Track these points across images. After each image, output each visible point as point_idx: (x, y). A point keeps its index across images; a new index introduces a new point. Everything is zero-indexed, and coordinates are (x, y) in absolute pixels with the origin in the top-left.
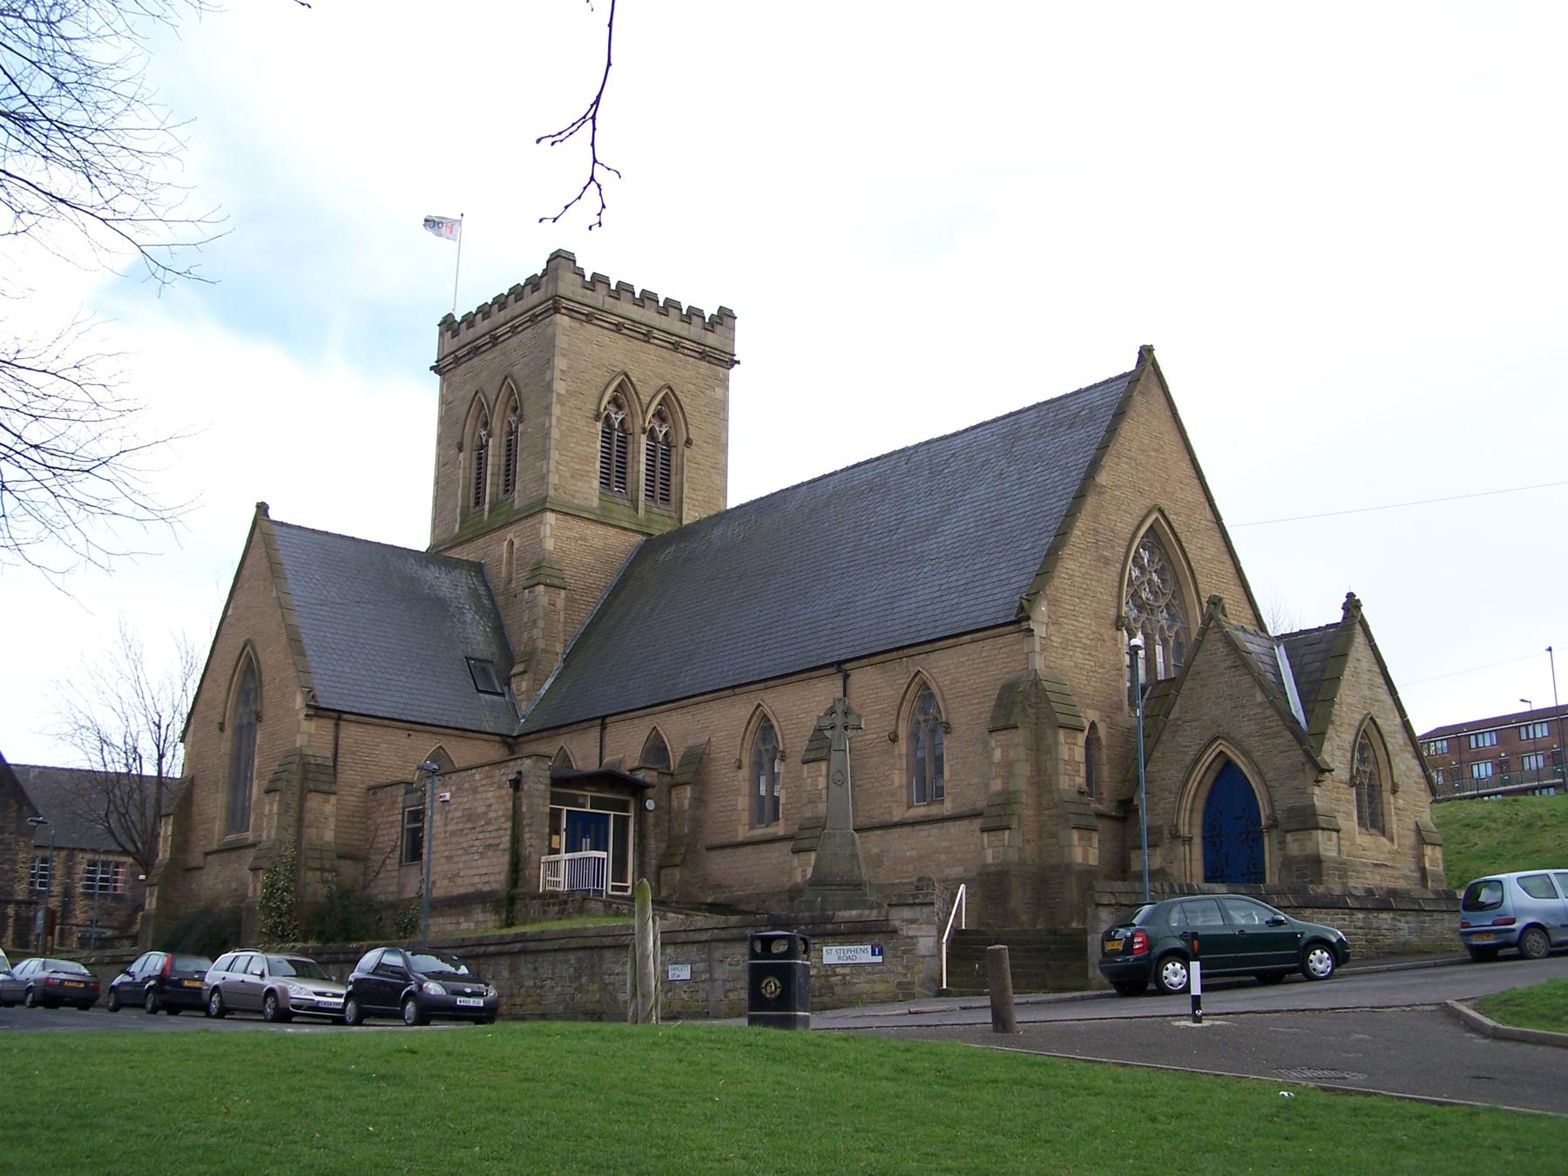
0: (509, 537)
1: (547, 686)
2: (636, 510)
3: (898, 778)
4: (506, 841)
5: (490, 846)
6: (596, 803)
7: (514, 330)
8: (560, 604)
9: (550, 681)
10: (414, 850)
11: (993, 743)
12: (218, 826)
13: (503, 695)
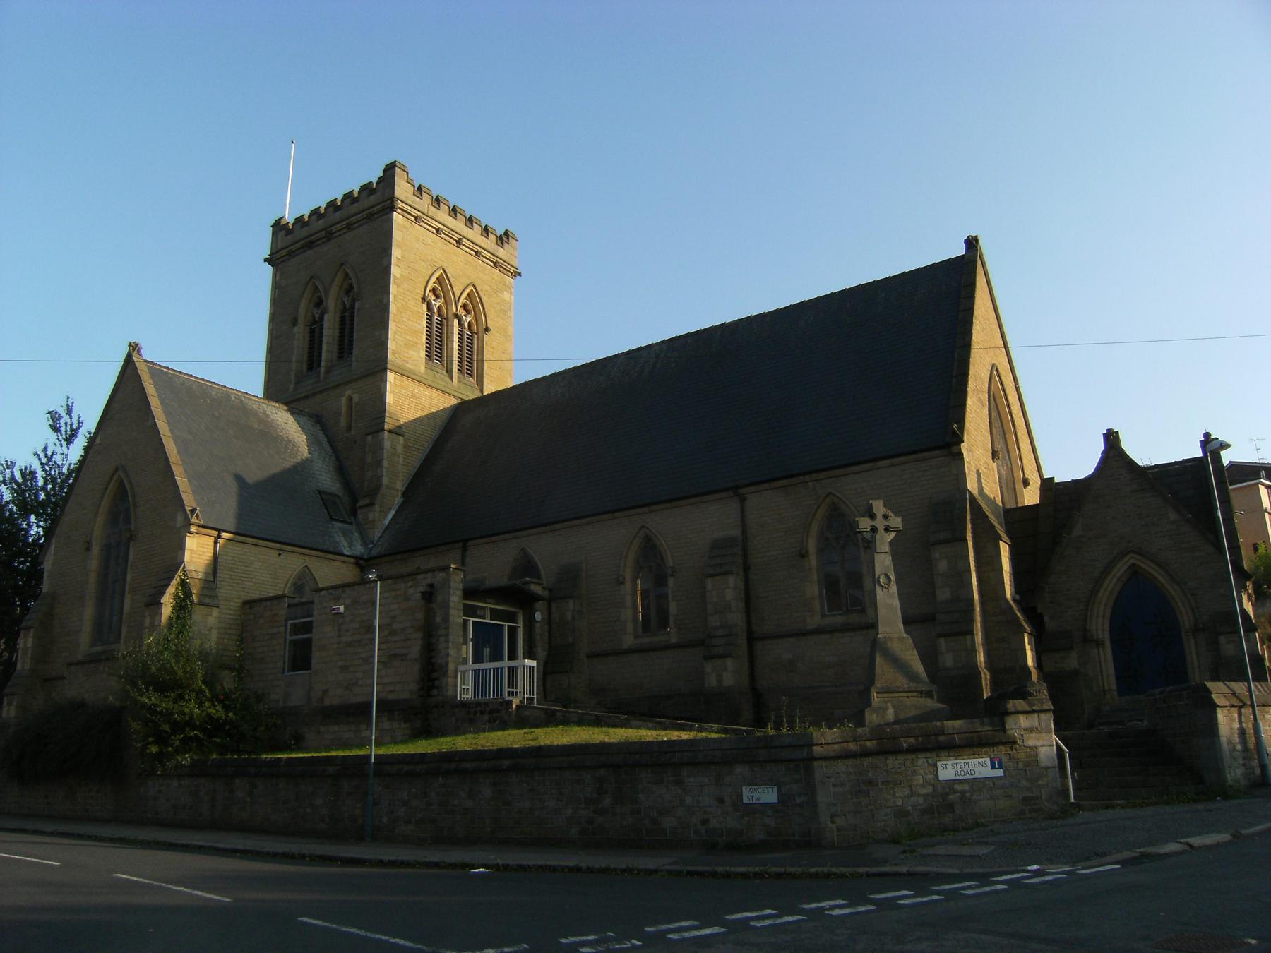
0: (348, 393)
1: (390, 517)
2: (451, 378)
3: (813, 589)
4: (415, 650)
5: (395, 656)
6: (495, 614)
7: (349, 227)
8: (400, 449)
9: (393, 512)
10: (301, 657)
11: (937, 555)
12: (85, 637)
13: (351, 524)
